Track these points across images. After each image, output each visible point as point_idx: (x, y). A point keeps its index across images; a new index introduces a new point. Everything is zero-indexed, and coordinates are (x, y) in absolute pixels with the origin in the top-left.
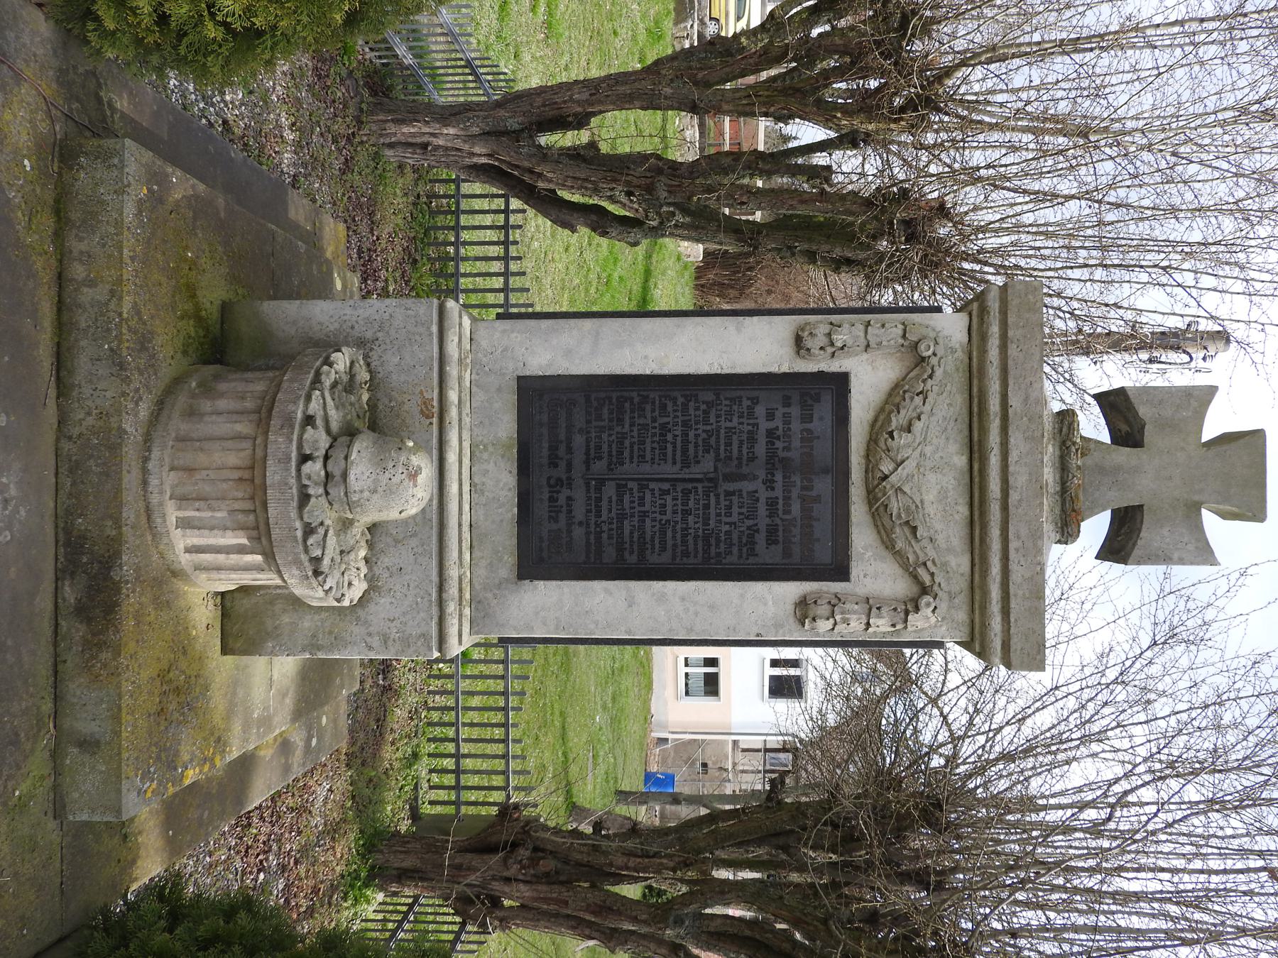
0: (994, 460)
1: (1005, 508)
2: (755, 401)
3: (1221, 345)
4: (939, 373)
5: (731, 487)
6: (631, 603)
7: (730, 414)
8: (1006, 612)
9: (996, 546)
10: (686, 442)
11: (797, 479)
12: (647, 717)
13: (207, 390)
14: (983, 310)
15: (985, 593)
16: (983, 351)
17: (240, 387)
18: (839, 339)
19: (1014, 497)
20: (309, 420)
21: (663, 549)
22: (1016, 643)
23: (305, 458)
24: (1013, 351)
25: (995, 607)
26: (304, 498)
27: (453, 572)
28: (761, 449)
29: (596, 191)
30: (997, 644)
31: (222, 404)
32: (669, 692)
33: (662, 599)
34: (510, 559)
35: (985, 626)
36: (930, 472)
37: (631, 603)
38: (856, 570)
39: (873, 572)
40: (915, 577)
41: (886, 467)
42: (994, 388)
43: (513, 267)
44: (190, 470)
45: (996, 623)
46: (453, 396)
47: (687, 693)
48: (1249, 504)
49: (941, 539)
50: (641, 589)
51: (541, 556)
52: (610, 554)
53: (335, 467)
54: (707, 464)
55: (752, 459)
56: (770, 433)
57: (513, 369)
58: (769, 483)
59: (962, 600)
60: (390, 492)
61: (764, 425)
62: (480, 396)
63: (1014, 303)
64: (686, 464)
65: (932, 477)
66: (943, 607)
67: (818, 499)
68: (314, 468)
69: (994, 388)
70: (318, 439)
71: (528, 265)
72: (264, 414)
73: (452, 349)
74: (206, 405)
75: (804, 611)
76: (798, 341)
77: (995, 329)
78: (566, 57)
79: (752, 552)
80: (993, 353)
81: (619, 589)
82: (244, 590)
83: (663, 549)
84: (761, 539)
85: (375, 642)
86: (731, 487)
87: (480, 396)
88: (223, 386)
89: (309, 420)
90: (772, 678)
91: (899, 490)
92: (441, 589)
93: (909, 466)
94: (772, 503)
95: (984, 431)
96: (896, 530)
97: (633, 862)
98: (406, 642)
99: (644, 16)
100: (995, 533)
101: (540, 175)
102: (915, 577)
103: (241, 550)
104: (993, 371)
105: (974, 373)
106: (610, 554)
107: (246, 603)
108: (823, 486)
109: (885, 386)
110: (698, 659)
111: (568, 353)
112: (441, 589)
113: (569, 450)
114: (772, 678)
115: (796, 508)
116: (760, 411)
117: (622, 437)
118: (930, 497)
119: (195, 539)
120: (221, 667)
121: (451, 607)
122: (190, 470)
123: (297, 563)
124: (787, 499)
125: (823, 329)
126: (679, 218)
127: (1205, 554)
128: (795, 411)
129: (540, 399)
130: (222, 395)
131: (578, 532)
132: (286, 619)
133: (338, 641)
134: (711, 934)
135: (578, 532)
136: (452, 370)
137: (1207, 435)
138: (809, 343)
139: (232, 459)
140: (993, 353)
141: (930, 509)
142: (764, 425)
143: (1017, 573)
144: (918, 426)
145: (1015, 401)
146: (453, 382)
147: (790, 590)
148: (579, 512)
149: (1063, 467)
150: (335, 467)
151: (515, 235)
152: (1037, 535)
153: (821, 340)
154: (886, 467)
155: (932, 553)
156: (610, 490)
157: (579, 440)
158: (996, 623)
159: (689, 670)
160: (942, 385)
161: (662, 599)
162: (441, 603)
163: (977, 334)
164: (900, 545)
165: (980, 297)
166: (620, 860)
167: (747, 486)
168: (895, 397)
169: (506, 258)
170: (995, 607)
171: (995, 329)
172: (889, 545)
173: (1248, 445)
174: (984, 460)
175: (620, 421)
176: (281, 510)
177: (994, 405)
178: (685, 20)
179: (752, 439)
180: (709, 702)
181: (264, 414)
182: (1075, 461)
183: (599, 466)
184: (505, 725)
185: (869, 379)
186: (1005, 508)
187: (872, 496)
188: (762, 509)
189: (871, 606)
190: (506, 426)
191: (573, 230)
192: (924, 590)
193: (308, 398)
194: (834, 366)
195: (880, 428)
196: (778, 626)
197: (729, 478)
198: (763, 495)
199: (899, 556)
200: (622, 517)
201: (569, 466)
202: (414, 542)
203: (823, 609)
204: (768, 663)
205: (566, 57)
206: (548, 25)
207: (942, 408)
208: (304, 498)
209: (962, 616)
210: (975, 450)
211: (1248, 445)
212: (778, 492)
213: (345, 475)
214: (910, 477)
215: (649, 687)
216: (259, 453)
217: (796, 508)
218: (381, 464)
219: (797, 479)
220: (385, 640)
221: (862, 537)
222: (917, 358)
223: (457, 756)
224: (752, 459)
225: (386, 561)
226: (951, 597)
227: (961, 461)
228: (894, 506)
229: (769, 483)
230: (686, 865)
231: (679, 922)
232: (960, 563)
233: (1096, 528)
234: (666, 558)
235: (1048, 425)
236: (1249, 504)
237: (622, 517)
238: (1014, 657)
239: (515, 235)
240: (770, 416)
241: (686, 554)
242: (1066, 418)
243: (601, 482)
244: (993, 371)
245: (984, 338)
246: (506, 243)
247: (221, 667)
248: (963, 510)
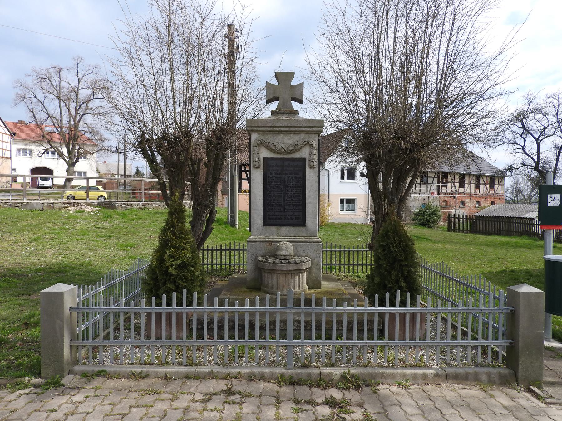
0: (282, 129)
1: (291, 127)
2: (269, 177)
3: (232, 27)
4: (264, 140)
5: (287, 182)
6: (310, 203)
7: (271, 182)
8: (312, 127)
9: (299, 129)
10: (277, 191)
11: (285, 168)
12: (362, 225)
13: (267, 286)
14: (252, 130)
15: (309, 131)
16: (260, 131)
17: (266, 279)
18: (257, 160)
19: (289, 125)
20: (274, 262)
21: (299, 196)
22: (319, 125)
23: (282, 263)
24: (260, 125)
25: (312, 129)
26: (289, 263)
27: (304, 240)
28: (279, 176)
29: (203, 221)
30: (319, 129)
31: (270, 282)
32: (353, 217)
33: (310, 196)
34: (301, 228)
35: (316, 131)
36: (284, 141)
37: (310, 203)
38: (304, 157)
39: (304, 153)
40: (305, 145)
41: (283, 150)
42: (267, 129)
43: (219, 248)
44: (283, 286)
45: (315, 129)
46: (267, 239)
47: (354, 210)
48: (291, 75)
49: (298, 140)
50: (308, 201)
51: (301, 222)
52: (300, 207)
53: (283, 258)
54: (282, 187)
55: (281, 178)
56: (276, 174)
57: (261, 227)
58: (286, 174)
59: (310, 136)
60: (288, 248)
61: (274, 175)
62: (267, 234)
63: (250, 125)
64: (282, 191)
65: (285, 141)
66: (311, 139)
67: (289, 164)
68: (283, 261)
69: (267, 129)
70: (277, 261)
71: (219, 244)
72: (272, 272)
73: (257, 240)
74: (270, 285)
75: (312, 167)
76: (257, 168)
77: (255, 128)
78: (140, 242)
79: (300, 178)
80: (260, 129)
81: (308, 205)
82: (307, 284)
83: (299, 196)
84: (297, 176)
85: (318, 256)
86: (287, 182)
87: (267, 234)
88: (266, 283)
89: (274, 262)
90: (347, 179)
91: (288, 148)
92: (307, 242)
93: (283, 146)
94: (290, 174)
95: (276, 131)
96: (296, 148)
97: (380, 212)
98: (318, 249)
99: (118, 219)
100: (296, 129)
101: (199, 236)
102: (305, 145)
103: (299, 278)
104: (264, 129)
105: (264, 133)
106: (300, 207)
107: (310, 284)
108: (287, 163)
109: (266, 150)
110: (341, 206)
111: (258, 216)
112: (307, 242)
113: (278, 215)
114: (347, 179)
115: (291, 169)
116: (271, 176)
117: (277, 205)
118: (289, 142)
119: (297, 287)
120: (323, 289)
121: (311, 240)
122: (283, 286)
123: (302, 265)
124: (289, 170)
125: (255, 163)
126: (211, 199)
127: (301, 85)
128: (271, 169)
129: (267, 222)
130: (268, 282)
131: (296, 214)
132: (314, 275)
133: (318, 264)
134: (396, 192)
135: (296, 214)
136: (262, 240)
137: (277, 84)
138: (257, 166)
139: (281, 278)
140: (260, 129)
141: (292, 141)
142: (274, 175)
143: (305, 125)
144: (275, 144)
145: (270, 125)
146: (264, 239)
147: (308, 170)
148: (292, 213)
149: (283, 114)
150: (283, 258)
151: (210, 248)
152: (297, 121)
153: (257, 163)
154: (283, 150)
155: (301, 142)
156: (287, 207)
157: (277, 214)
158: (315, 129)
159: (345, 210)
160: (266, 139)
161: (310, 196)
162: (310, 242)
163: (256, 132)
164: (299, 148)
165: (248, 131)
166: (380, 215)
167: (286, 179)
168: (269, 148)
169: (217, 250)
170: (312, 129)
171: (255, 128)
172: (299, 150)
173: (278, 75)
174: (282, 131)
175: (272, 205)
176: (292, 267)
177: (271, 129)
178: (115, 206)
179: (277, 177)
180: (357, 202)
181: (272, 272)
182: (282, 111)
183: (282, 209)
184: (349, 251)
185: (265, 153)
186: (291, 127)
187: (289, 153)
188: (291, 176)
189: (311, 154)
190: (273, 229)
191: (213, 228)
192: (308, 143)
193: (270, 263)
194: (262, 160)
195: (275, 152)
196: (315, 173)
197: (285, 182)
198: (288, 175)
199: (301, 148)
200: (293, 205)
201: (282, 216)
202: (298, 248)
203: (312, 163)
204: (342, 181)
205: (140, 242)
206: (131, 247)
207: (271, 139)
208: (289, 263)
209: (313, 136)
210: (280, 132)
211: (278, 75)
212: (288, 172)
213: (285, 256)
214: (285, 146)
215: (350, 224)
216: (280, 272)
217: (291, 169)
218: (282, 249)
219: (285, 168)
220: (318, 254)
221: (297, 155)
222: (262, 144)
223: (358, 265)
224: (281, 178)
225: (302, 253)
226: (309, 138)
227: (282, 135)
228: (291, 149)
229: (286, 174)
230: (381, 198)
231: (393, 199)
232: (303, 136)
233: (295, 105)
234: (301, 196)
235: (274, 118)
236: (291, 75)
237: (293, 205)
238: (322, 126)
239: (210, 248)
240: (272, 174)
241: (300, 191)
242: (273, 113)
243: (285, 209)
244: (264, 129)
245: (257, 130)
246: (212, 250)
247: (323, 289)
248: (292, 135)
